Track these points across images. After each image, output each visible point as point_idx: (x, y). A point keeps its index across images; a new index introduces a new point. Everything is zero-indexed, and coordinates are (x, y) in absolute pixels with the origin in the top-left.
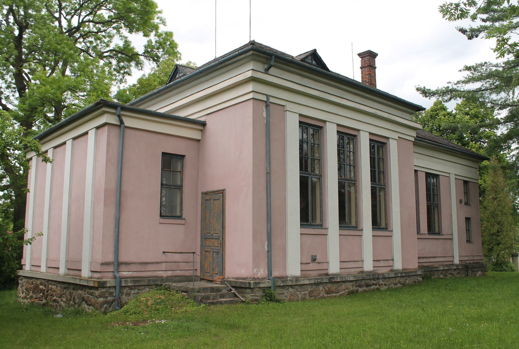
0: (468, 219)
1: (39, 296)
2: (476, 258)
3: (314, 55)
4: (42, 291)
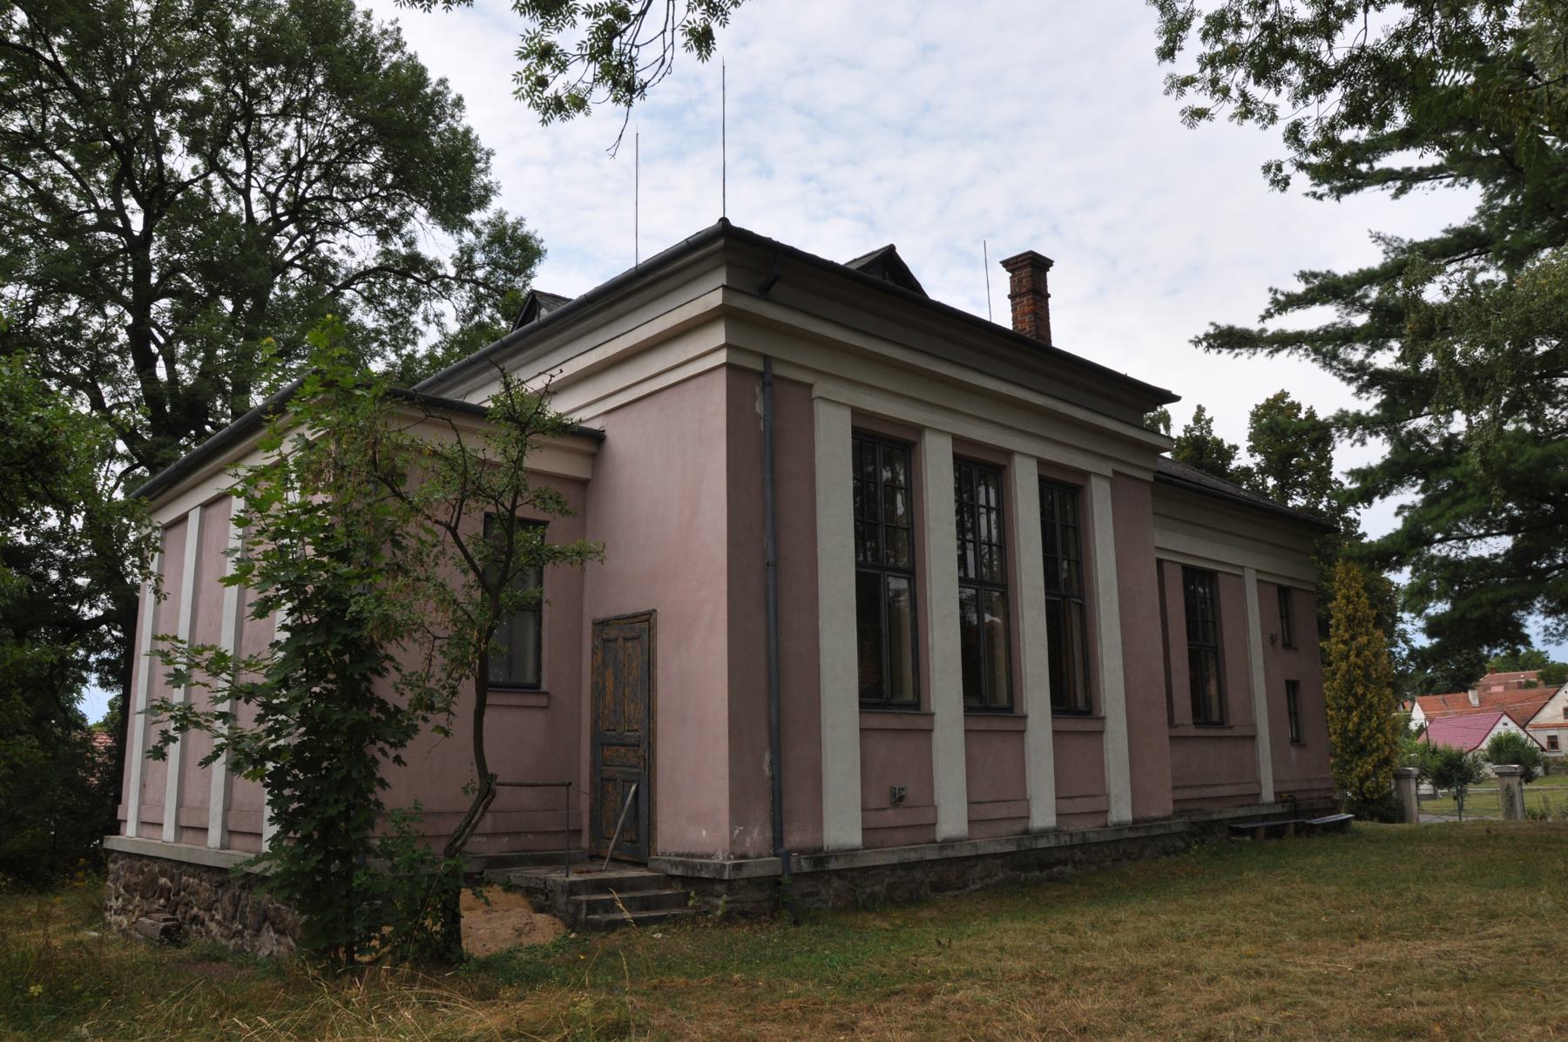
0: (1292, 686)
1: (156, 906)
2: (1315, 785)
3: (888, 260)
4: (164, 892)
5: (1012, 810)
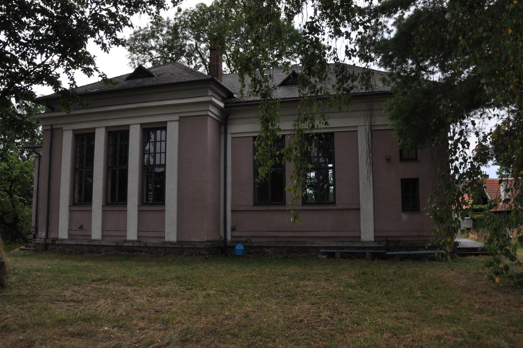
5: (121, 234)
